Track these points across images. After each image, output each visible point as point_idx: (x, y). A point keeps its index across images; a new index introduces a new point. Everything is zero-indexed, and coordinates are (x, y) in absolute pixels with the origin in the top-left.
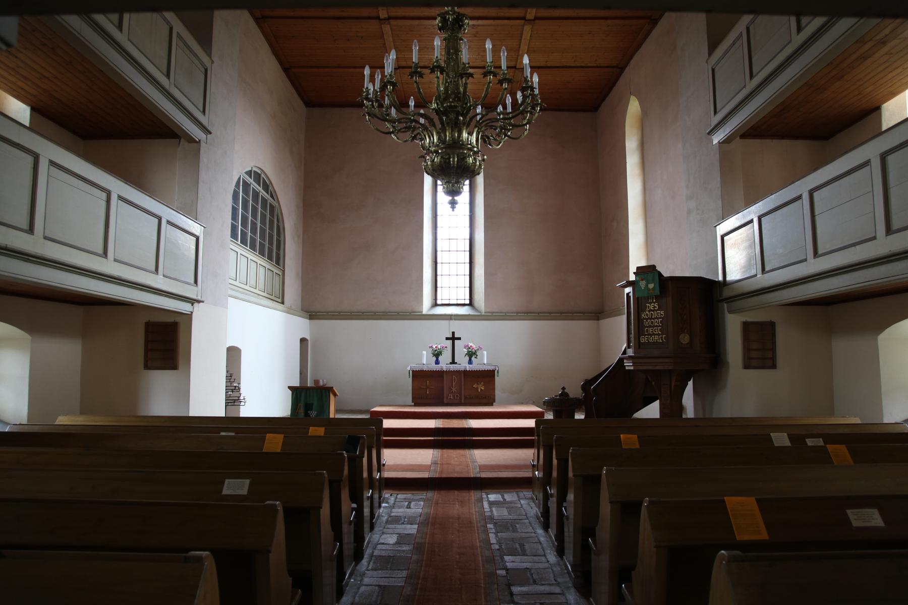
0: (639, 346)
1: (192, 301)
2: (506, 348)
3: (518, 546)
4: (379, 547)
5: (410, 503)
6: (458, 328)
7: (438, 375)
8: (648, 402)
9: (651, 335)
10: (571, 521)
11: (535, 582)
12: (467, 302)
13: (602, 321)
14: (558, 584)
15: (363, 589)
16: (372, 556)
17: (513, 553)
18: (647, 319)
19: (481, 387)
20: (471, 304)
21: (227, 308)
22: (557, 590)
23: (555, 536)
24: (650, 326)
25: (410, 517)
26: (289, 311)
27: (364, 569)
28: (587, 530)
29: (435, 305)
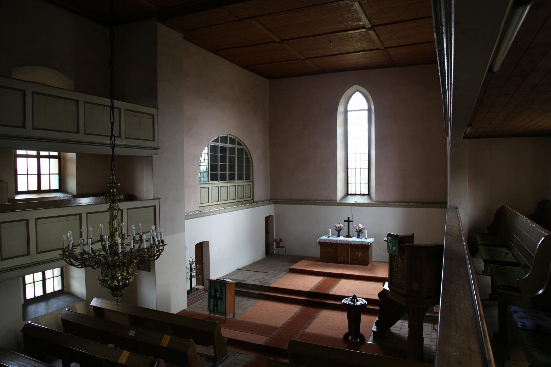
20: (369, 194)
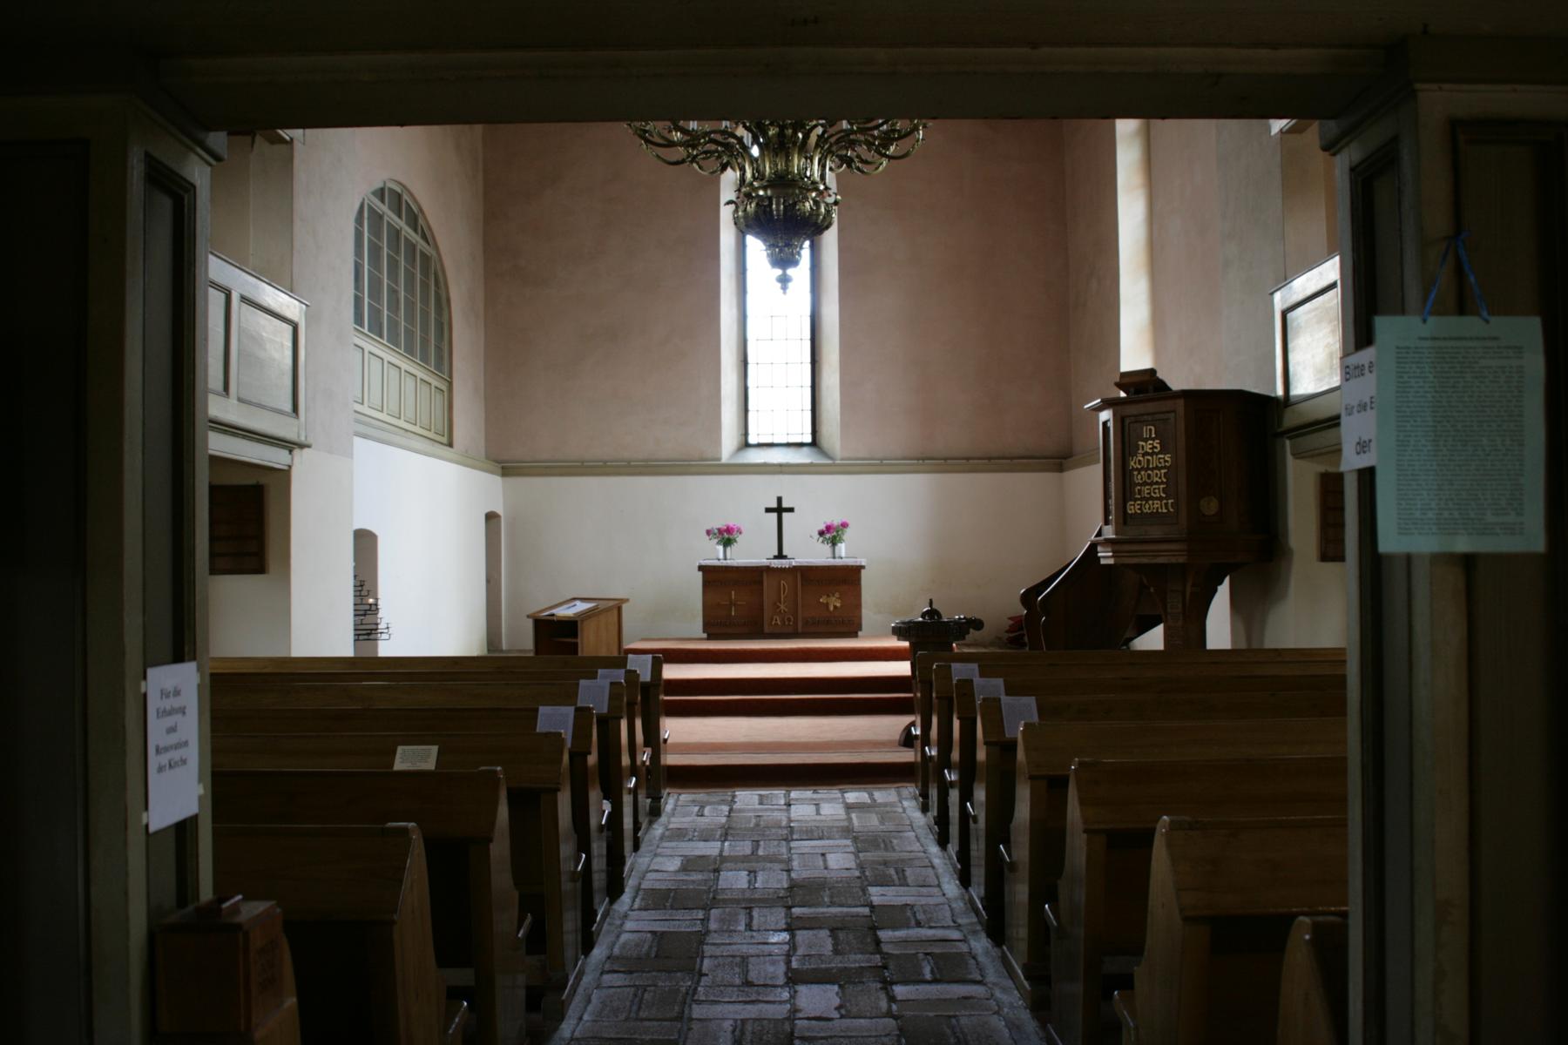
0: (1125, 519)
1: (290, 445)
2: (887, 531)
3: (892, 871)
4: (650, 876)
5: (702, 807)
6: (789, 489)
7: (753, 576)
8: (1145, 626)
9: (1147, 500)
10: (1024, 872)
11: (919, 924)
12: (808, 439)
13: (1066, 474)
14: (958, 927)
15: (624, 937)
16: (638, 889)
17: (883, 882)
18: (1139, 470)
19: (834, 602)
20: (814, 443)
21: (351, 455)
22: (956, 935)
23: (1025, 968)
24: (1145, 484)
25: (702, 831)
26: (467, 461)
27: (626, 908)
28: (1000, 828)
29: (746, 445)
